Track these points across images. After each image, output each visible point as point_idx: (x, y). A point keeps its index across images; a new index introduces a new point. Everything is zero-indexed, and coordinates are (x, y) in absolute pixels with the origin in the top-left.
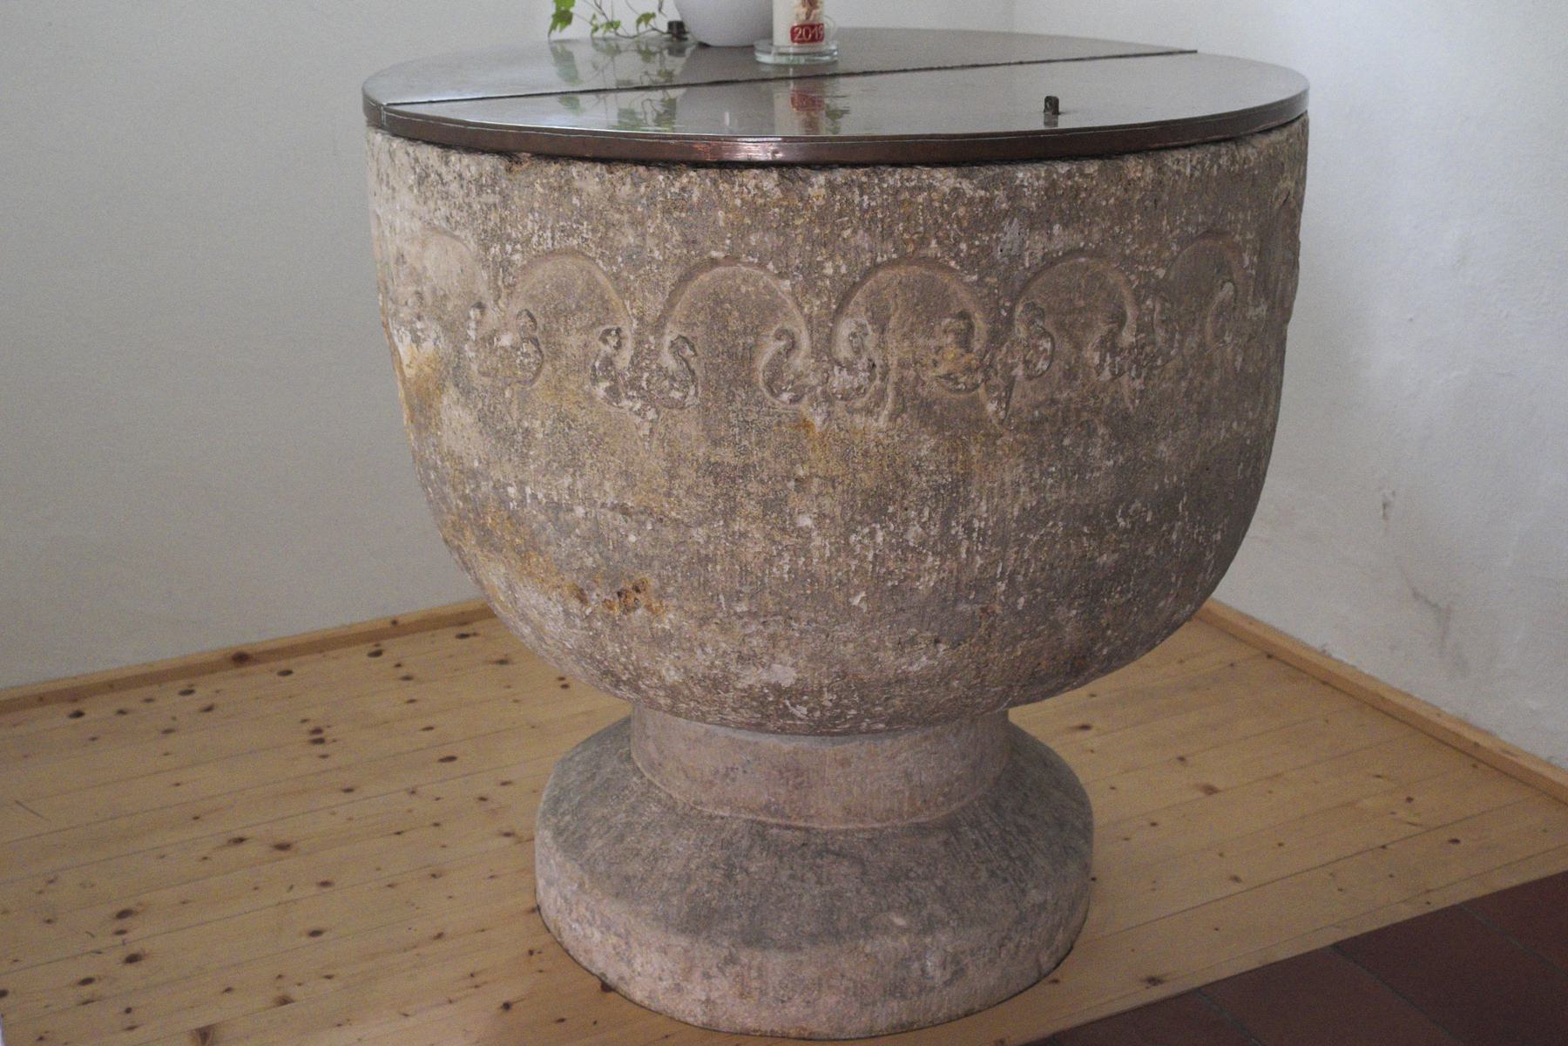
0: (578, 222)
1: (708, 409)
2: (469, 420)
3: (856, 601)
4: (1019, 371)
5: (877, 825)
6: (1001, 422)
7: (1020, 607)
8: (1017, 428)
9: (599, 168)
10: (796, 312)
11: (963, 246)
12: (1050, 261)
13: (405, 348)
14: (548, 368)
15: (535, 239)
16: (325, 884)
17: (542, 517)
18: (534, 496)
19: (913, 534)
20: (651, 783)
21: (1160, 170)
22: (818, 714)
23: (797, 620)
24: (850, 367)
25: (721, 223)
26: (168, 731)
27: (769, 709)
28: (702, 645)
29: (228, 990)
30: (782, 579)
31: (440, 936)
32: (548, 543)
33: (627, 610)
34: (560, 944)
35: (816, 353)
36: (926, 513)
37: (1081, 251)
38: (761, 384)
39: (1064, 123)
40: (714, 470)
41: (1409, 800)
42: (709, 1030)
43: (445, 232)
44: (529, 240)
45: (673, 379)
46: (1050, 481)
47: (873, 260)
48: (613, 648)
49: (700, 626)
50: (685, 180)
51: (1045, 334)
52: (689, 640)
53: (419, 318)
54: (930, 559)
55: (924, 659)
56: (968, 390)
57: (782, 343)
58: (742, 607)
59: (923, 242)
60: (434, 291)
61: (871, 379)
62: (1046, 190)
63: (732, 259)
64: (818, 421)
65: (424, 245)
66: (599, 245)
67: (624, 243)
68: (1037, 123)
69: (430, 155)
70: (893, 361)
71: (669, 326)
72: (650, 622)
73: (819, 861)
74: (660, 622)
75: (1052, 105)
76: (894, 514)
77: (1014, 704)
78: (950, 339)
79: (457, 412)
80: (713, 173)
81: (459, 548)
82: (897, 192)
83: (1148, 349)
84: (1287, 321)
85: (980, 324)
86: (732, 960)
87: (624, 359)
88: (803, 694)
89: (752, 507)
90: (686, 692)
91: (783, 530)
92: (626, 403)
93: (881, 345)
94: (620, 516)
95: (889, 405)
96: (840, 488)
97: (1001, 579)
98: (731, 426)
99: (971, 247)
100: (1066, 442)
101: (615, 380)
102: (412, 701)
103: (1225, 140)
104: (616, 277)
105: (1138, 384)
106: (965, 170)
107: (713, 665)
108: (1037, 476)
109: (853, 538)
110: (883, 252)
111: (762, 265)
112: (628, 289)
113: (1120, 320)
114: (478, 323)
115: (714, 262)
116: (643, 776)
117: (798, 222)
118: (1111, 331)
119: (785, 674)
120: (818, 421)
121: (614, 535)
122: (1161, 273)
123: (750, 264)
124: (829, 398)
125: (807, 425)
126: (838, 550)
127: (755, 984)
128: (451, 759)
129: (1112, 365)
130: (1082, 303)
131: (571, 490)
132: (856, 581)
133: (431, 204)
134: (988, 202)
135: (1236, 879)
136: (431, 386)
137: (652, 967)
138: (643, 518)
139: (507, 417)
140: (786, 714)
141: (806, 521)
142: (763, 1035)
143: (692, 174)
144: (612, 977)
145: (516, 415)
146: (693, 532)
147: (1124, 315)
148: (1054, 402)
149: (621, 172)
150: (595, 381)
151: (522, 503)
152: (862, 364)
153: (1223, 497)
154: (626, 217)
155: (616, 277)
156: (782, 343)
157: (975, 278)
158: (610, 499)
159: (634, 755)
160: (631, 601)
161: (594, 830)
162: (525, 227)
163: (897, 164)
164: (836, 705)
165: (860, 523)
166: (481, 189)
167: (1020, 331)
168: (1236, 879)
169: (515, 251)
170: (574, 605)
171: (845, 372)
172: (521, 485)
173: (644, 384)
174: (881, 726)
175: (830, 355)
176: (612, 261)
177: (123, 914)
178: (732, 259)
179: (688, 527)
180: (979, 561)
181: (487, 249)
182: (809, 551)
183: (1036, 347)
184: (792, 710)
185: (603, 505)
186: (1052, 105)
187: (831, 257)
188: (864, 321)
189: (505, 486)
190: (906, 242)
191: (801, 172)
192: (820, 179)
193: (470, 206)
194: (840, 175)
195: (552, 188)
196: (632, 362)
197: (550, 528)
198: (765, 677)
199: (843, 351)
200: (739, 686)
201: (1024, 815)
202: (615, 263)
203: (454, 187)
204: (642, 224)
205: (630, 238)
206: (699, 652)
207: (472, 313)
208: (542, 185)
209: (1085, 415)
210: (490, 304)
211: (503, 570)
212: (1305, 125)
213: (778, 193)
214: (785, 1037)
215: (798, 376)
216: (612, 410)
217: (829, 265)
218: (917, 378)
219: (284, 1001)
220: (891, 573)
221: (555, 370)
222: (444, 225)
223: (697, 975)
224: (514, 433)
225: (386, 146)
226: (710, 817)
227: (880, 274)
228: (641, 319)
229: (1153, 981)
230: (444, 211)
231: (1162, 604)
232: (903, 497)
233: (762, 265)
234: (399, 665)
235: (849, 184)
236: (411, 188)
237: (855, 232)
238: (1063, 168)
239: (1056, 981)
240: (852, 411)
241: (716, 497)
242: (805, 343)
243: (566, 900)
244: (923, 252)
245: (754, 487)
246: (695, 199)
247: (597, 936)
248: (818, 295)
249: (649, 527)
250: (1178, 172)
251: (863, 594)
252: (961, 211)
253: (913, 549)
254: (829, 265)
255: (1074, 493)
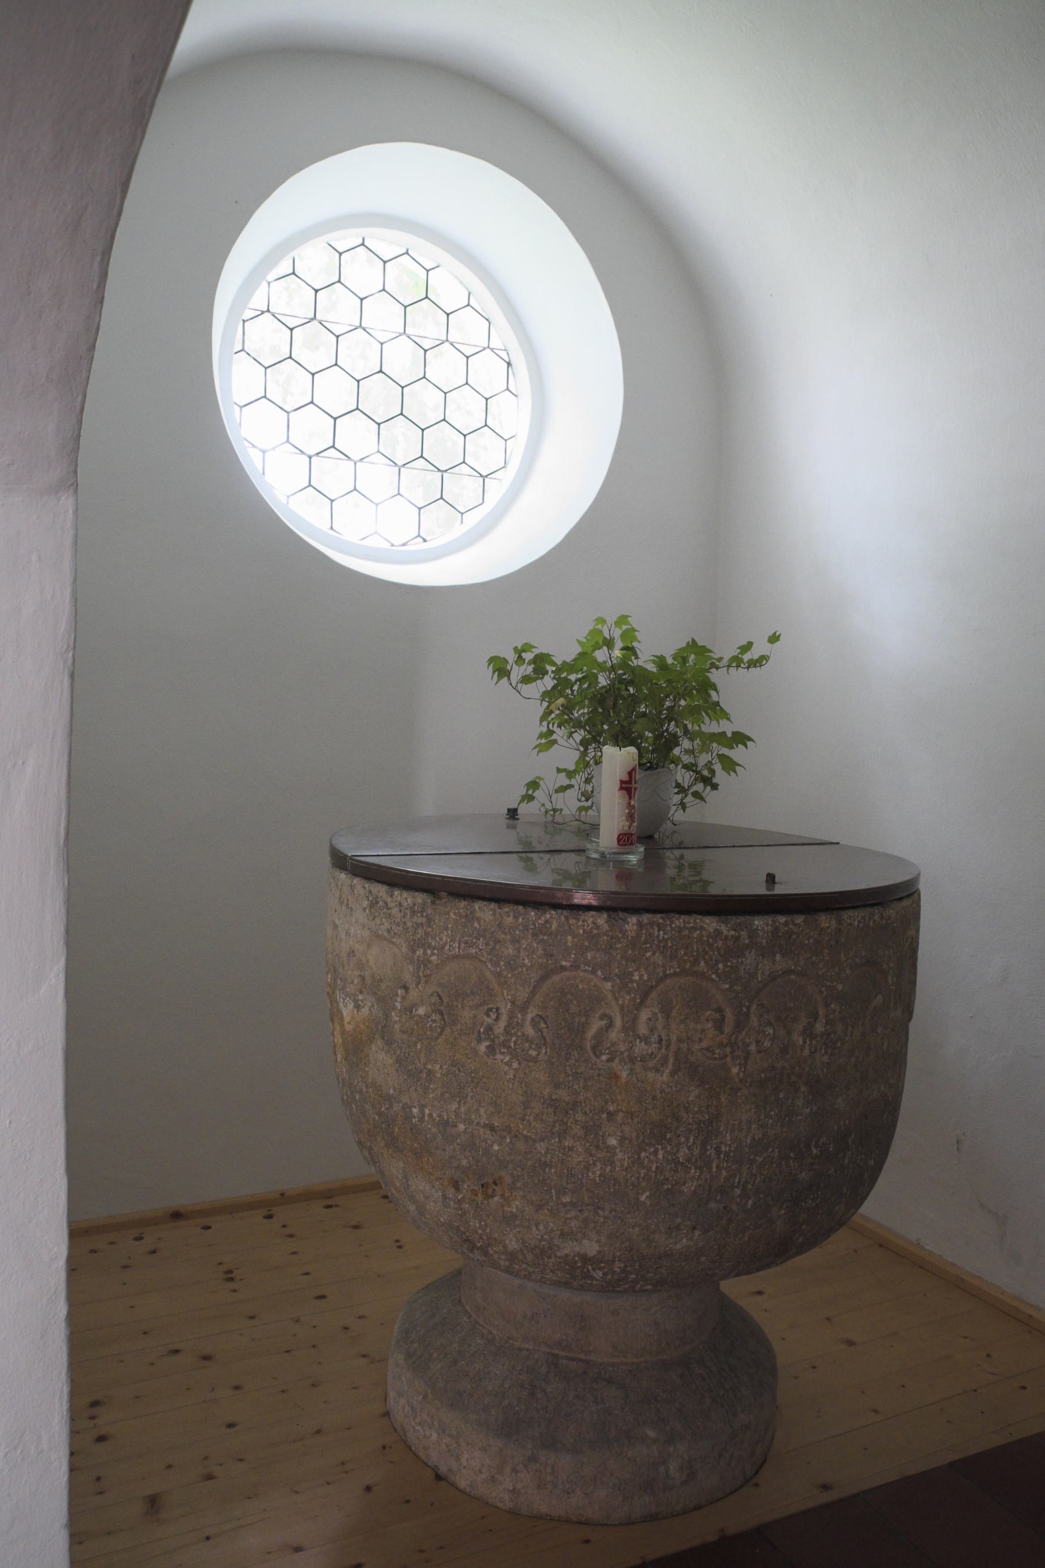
0: (476, 938)
1: (552, 1063)
2: (390, 1061)
3: (643, 1198)
4: (753, 1048)
5: (635, 1360)
6: (741, 1081)
7: (749, 1206)
8: (751, 1085)
9: (493, 905)
10: (613, 1003)
11: (721, 966)
12: (773, 977)
13: (347, 1010)
14: (448, 1030)
15: (447, 947)
16: (237, 1388)
17: (434, 1130)
18: (430, 1115)
19: (683, 1153)
20: (477, 1322)
21: (840, 922)
22: (609, 1277)
23: (603, 1209)
24: (646, 1040)
25: (569, 944)
26: (125, 1267)
27: (576, 1273)
28: (537, 1225)
29: (170, 1466)
30: (594, 1180)
31: (319, 1432)
32: (437, 1148)
33: (488, 1197)
34: (405, 1442)
35: (625, 1029)
36: (691, 1140)
37: (791, 972)
38: (588, 1048)
39: (779, 890)
40: (552, 1103)
41: (989, 1356)
42: (513, 1513)
43: (385, 939)
44: (443, 948)
45: (531, 1042)
46: (771, 1121)
47: (664, 972)
48: (475, 1223)
49: (537, 1211)
50: (548, 916)
51: (769, 1024)
52: (528, 1220)
53: (361, 992)
54: (693, 1171)
55: (684, 1241)
56: (720, 1059)
57: (604, 1022)
58: (566, 1199)
59: (696, 962)
60: (373, 977)
61: (660, 1049)
62: (772, 932)
63: (575, 967)
64: (624, 1075)
65: (369, 946)
66: (489, 954)
67: (506, 953)
68: (761, 890)
69: (380, 890)
70: (674, 1038)
71: (531, 1008)
72: (503, 1206)
73: (595, 1386)
74: (509, 1206)
75: (771, 879)
76: (670, 1139)
77: (725, 1277)
78: (710, 1025)
79: (382, 1056)
80: (566, 913)
81: (370, 1149)
82: (680, 930)
83: (832, 1036)
84: (910, 1020)
85: (729, 1014)
86: (533, 1459)
87: (500, 1028)
88: (601, 1262)
89: (578, 1130)
90: (521, 1257)
91: (598, 1147)
92: (499, 1057)
93: (666, 1026)
94: (489, 1132)
95: (670, 1066)
96: (636, 1120)
97: (738, 1187)
98: (568, 1075)
99: (725, 966)
100: (781, 1095)
101: (492, 1041)
102: (294, 1253)
103: (878, 904)
104: (499, 975)
105: (826, 1059)
106: (723, 918)
107: (542, 1239)
108: (762, 1117)
109: (643, 1154)
110: (671, 967)
111: (593, 972)
112: (506, 982)
113: (815, 1016)
114: (403, 998)
115: (563, 969)
116: (470, 1317)
117: (619, 946)
118: (809, 1023)
119: (591, 1247)
120: (624, 1075)
121: (484, 1145)
122: (840, 987)
123: (586, 971)
124: (632, 1060)
125: (617, 1077)
126: (633, 1163)
127: (549, 1478)
128: (323, 1297)
129: (811, 1044)
130: (792, 1005)
131: (457, 1113)
132: (644, 1184)
133: (378, 921)
134: (737, 939)
135: (876, 1411)
136: (364, 1038)
137: (476, 1463)
138: (504, 1134)
139: (417, 1061)
140: (587, 1276)
141: (613, 1142)
142: (552, 1519)
143: (553, 912)
144: (443, 1469)
145: (423, 1060)
146: (538, 1146)
147: (817, 1013)
148: (773, 1068)
149: (506, 909)
150: (480, 1040)
151: (421, 1119)
152: (654, 1038)
153: (871, 1133)
154: (508, 937)
155: (499, 975)
156: (604, 1022)
157: (727, 986)
158: (483, 1120)
159: (463, 1300)
160: (490, 1191)
161: (435, 1355)
162: (441, 939)
163: (681, 912)
164: (623, 1271)
165: (647, 1144)
166: (414, 913)
167: (754, 1021)
168: (876, 1411)
169: (433, 954)
170: (451, 1192)
171: (643, 1043)
172: (422, 1107)
173: (512, 1045)
174: (649, 1287)
175: (634, 1031)
176: (496, 964)
177: (95, 1404)
178: (575, 967)
179: (534, 1141)
180: (724, 1173)
181: (414, 952)
182: (613, 1162)
183: (764, 1032)
184: (593, 1273)
185: (478, 1124)
186: (771, 879)
187: (638, 969)
188: (657, 1011)
189: (410, 1108)
190: (685, 962)
191: (621, 914)
192: (633, 919)
193: (405, 923)
194: (646, 918)
195: (461, 916)
196: (505, 1030)
197: (439, 1138)
198: (577, 1249)
199: (643, 1029)
200: (559, 1254)
201: (728, 1359)
202: (499, 965)
203: (395, 911)
204: (518, 942)
205: (511, 951)
206: (534, 1228)
207: (399, 992)
208: (455, 914)
209: (793, 1078)
210: (412, 986)
211: (402, 1165)
212: (919, 896)
213: (606, 927)
214: (567, 1521)
215: (613, 1044)
216: (490, 1061)
217: (636, 973)
218: (689, 1049)
219: (210, 1477)
220: (666, 1179)
221: (453, 1032)
222: (386, 934)
223: (508, 1470)
224: (421, 1072)
225: (349, 882)
226: (520, 1349)
227: (668, 981)
228: (513, 1003)
229: (826, 1487)
230: (387, 925)
231: (837, 1208)
232: (677, 1128)
233: (593, 972)
234: (284, 1226)
235: (651, 924)
236: (364, 909)
237: (654, 953)
238: (782, 919)
239: (756, 1485)
240: (646, 1069)
241: (555, 1122)
242: (618, 1022)
243: (412, 1408)
244: (696, 968)
245: (580, 1117)
246: (554, 928)
247: (435, 1436)
248: (629, 993)
249: (508, 1140)
250: (850, 924)
251: (648, 1193)
252: (720, 944)
253: (682, 1164)
254: (636, 973)
255: (785, 1129)
